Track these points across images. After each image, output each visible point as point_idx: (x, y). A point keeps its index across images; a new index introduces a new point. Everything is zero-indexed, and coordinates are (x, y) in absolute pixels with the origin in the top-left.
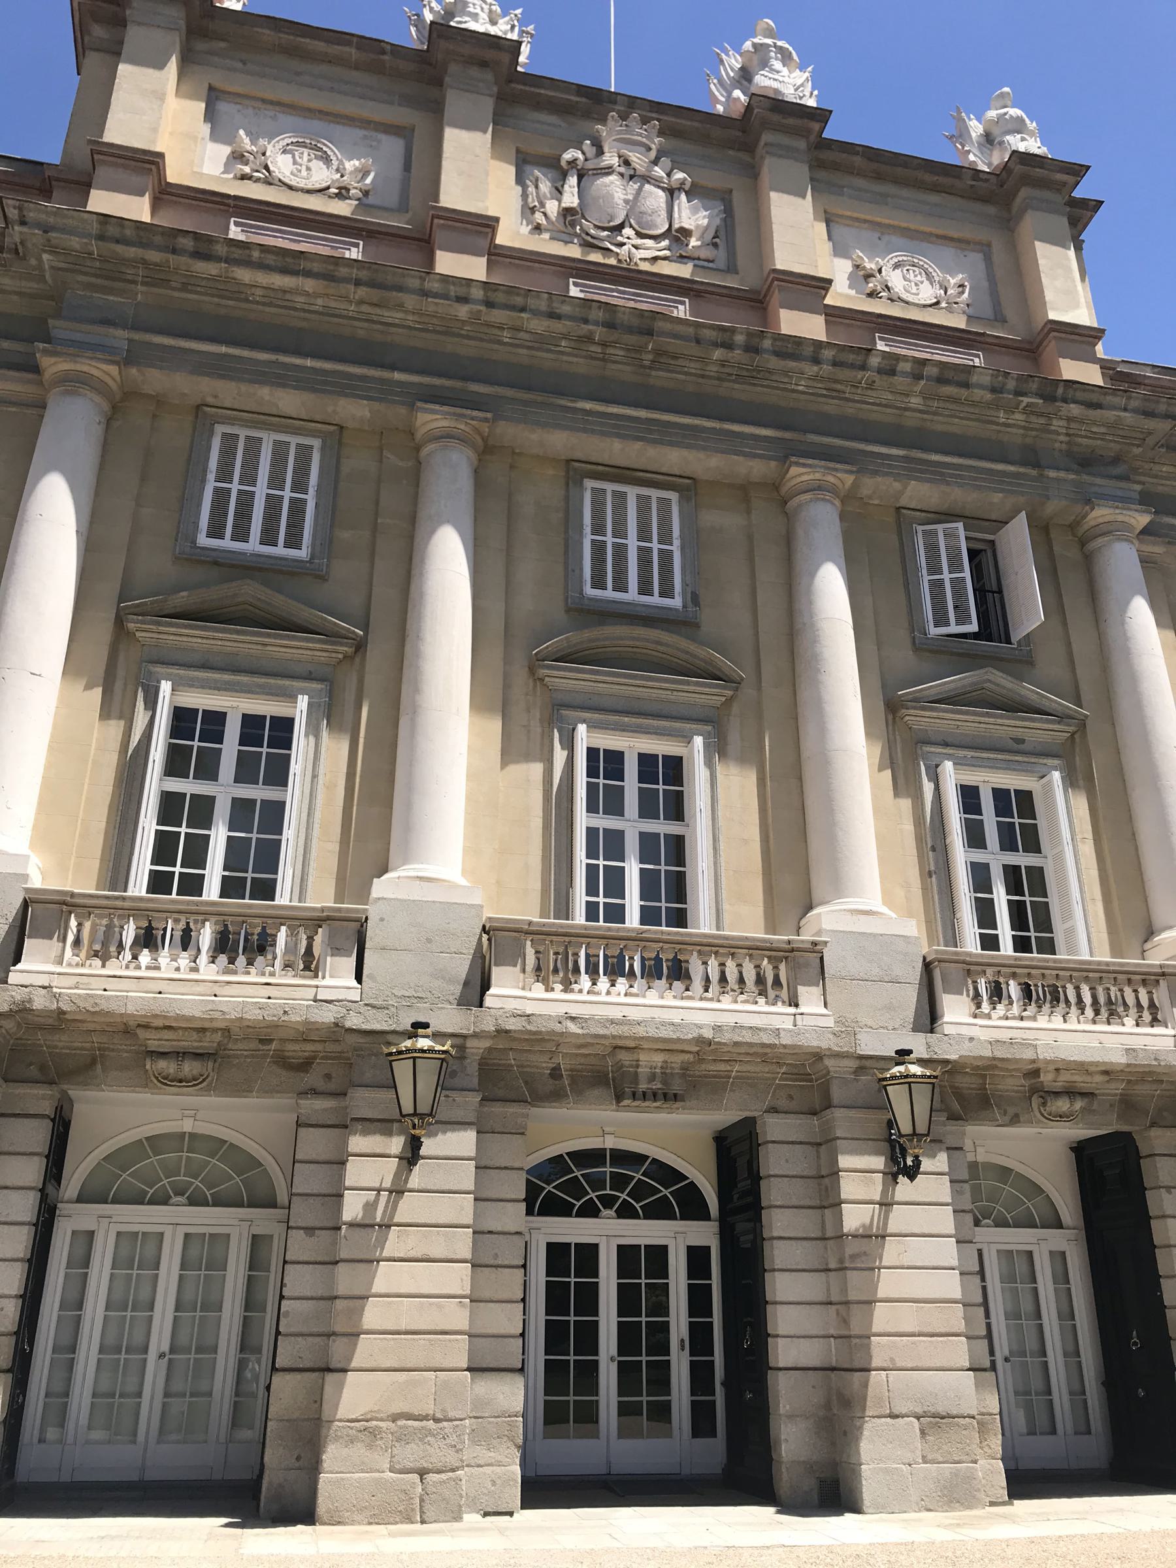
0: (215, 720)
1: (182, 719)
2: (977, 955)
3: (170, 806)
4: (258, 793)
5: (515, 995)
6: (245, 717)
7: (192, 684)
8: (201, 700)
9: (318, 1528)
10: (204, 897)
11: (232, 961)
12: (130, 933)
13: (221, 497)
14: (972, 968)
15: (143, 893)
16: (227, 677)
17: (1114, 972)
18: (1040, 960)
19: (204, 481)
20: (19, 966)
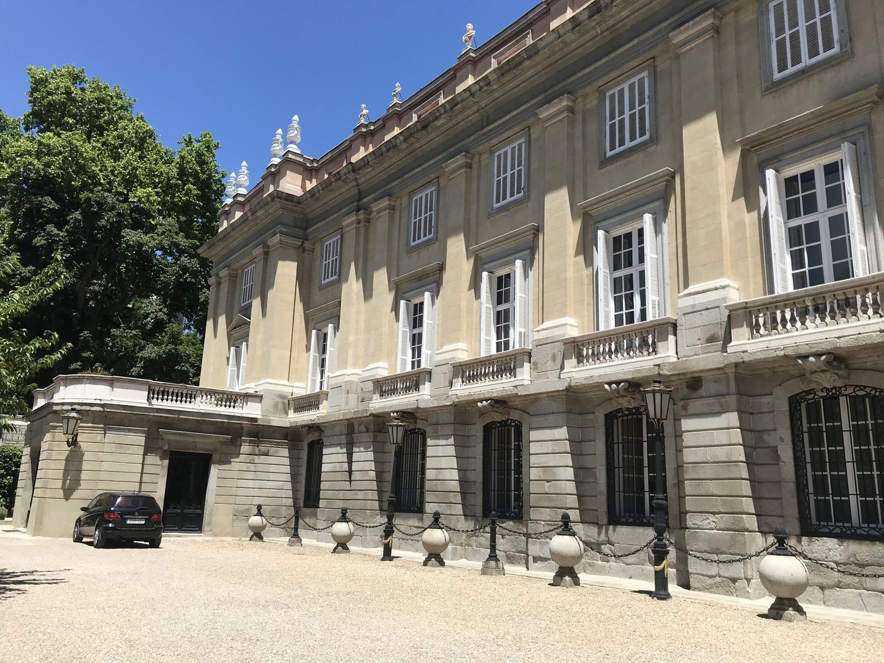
0: (808, 177)
1: (790, 185)
2: (793, 293)
3: (794, 236)
4: (802, 221)
5: (746, 344)
6: (825, 167)
7: (615, 225)
8: (621, 231)
9: (783, 621)
10: (648, 320)
11: (823, 319)
12: (637, 342)
13: (781, 45)
14: (835, 293)
15: (791, 289)
16: (618, 218)
17: (802, 297)
18: (814, 290)
19: (770, 41)
20: (731, 344)
